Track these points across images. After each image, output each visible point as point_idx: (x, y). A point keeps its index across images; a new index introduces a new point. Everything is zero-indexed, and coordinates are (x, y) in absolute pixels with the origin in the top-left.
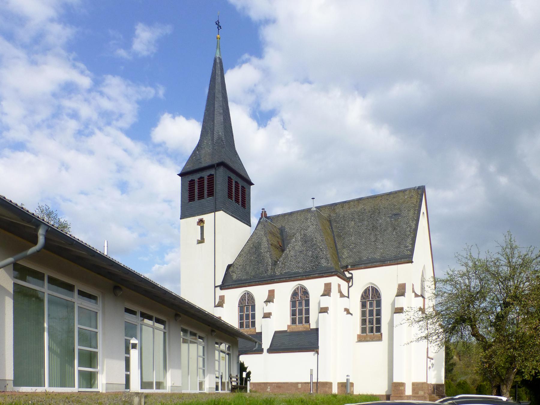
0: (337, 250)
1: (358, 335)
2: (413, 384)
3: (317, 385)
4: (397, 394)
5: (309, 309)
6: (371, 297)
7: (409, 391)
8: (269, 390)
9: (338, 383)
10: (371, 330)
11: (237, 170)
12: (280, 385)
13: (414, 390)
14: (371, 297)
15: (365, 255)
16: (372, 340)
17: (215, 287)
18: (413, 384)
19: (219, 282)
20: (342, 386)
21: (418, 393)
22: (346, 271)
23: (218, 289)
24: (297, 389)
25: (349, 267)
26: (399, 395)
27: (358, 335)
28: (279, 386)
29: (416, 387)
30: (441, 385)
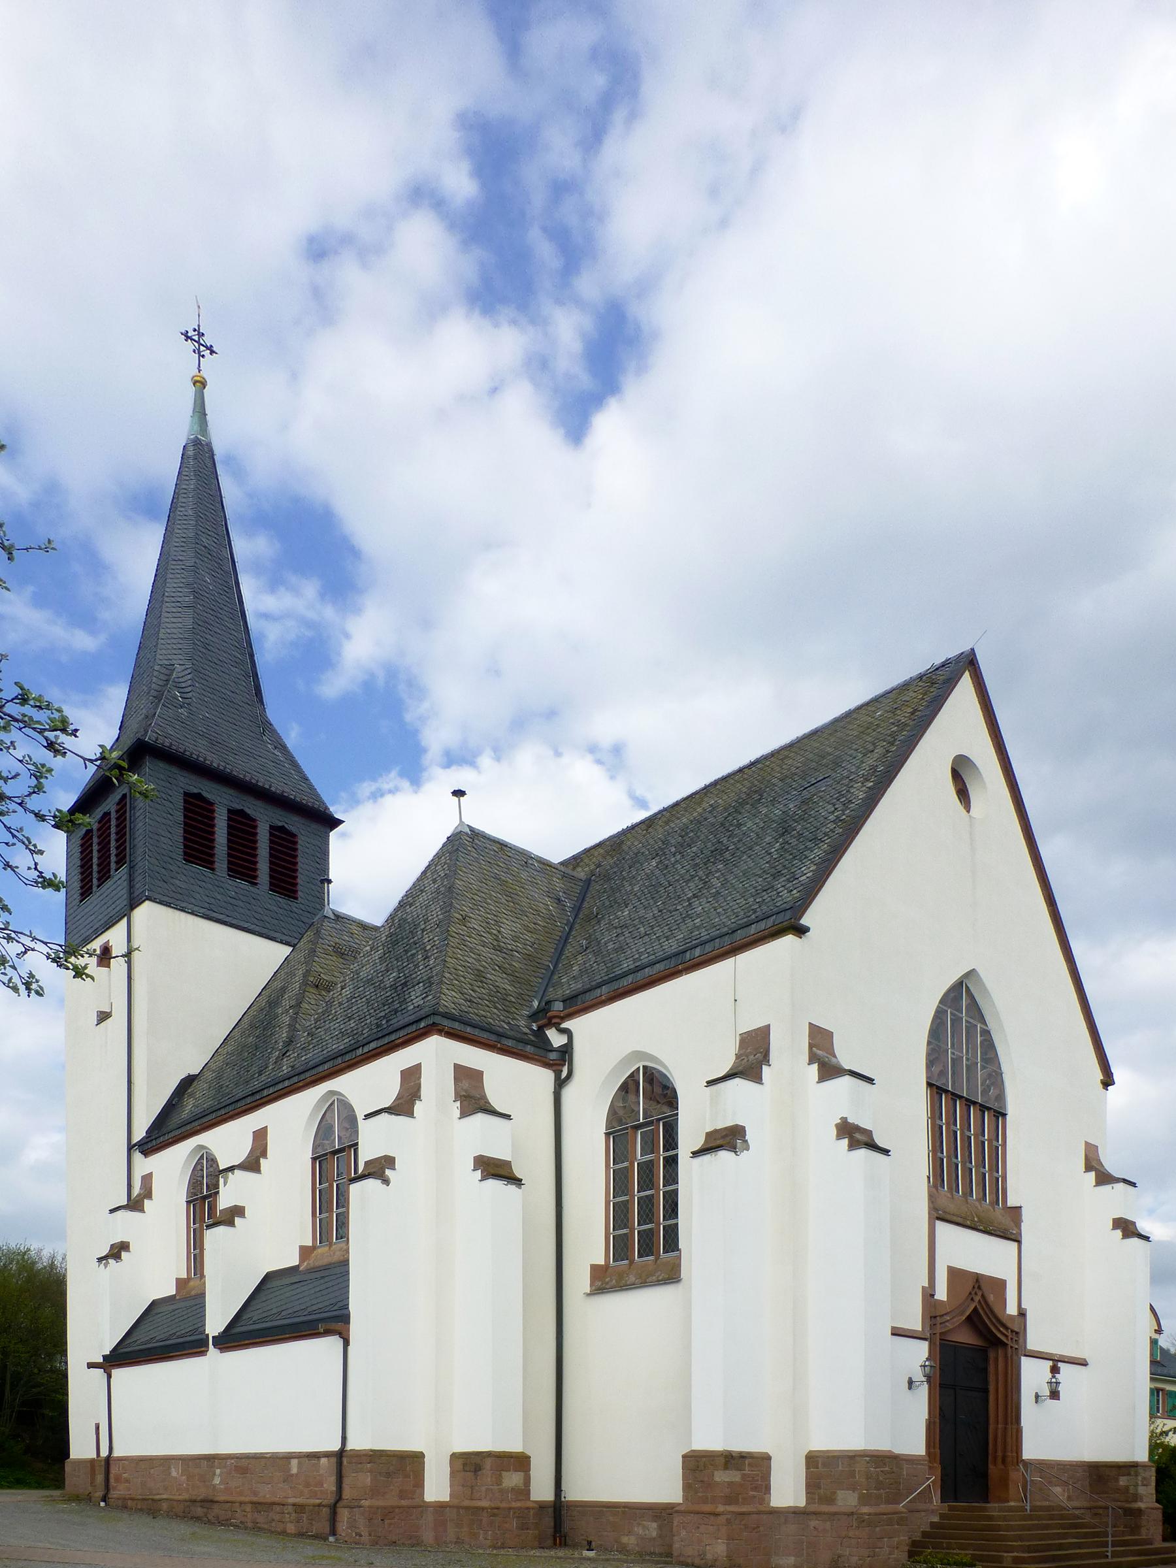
0: (561, 954)
1: (594, 1268)
2: (813, 1460)
3: (340, 1464)
4: (705, 1501)
5: (676, 1192)
6: (647, 1103)
7: (437, 1487)
8: (217, 1481)
9: (454, 1457)
10: (647, 1248)
11: (174, 769)
12: (244, 1463)
13: (813, 1485)
14: (647, 1103)
15: (639, 951)
16: (645, 1281)
17: (130, 1148)
18: (813, 1460)
19: (139, 1134)
20: (459, 1465)
21: (830, 1500)
22: (550, 1024)
23: (137, 1156)
24: (288, 1478)
25: (558, 1006)
26: (707, 1508)
27: (594, 1268)
28: (244, 1464)
29: (822, 1469)
30: (883, 1465)
